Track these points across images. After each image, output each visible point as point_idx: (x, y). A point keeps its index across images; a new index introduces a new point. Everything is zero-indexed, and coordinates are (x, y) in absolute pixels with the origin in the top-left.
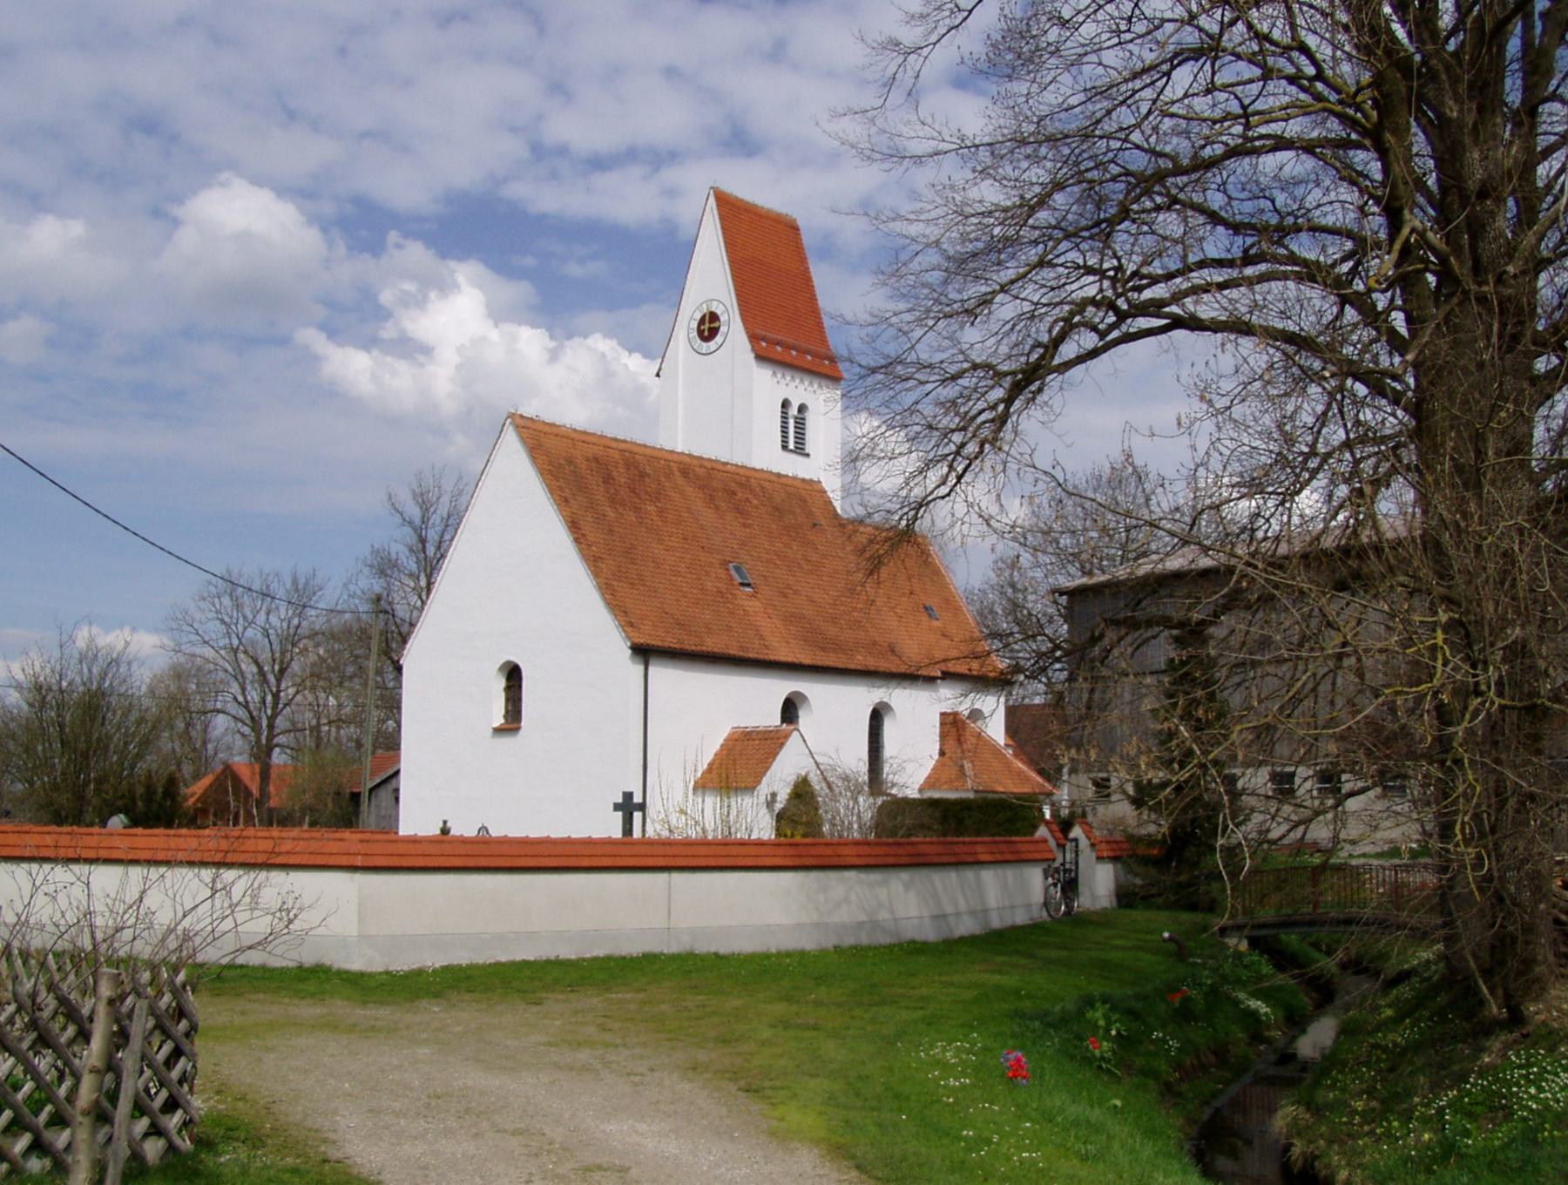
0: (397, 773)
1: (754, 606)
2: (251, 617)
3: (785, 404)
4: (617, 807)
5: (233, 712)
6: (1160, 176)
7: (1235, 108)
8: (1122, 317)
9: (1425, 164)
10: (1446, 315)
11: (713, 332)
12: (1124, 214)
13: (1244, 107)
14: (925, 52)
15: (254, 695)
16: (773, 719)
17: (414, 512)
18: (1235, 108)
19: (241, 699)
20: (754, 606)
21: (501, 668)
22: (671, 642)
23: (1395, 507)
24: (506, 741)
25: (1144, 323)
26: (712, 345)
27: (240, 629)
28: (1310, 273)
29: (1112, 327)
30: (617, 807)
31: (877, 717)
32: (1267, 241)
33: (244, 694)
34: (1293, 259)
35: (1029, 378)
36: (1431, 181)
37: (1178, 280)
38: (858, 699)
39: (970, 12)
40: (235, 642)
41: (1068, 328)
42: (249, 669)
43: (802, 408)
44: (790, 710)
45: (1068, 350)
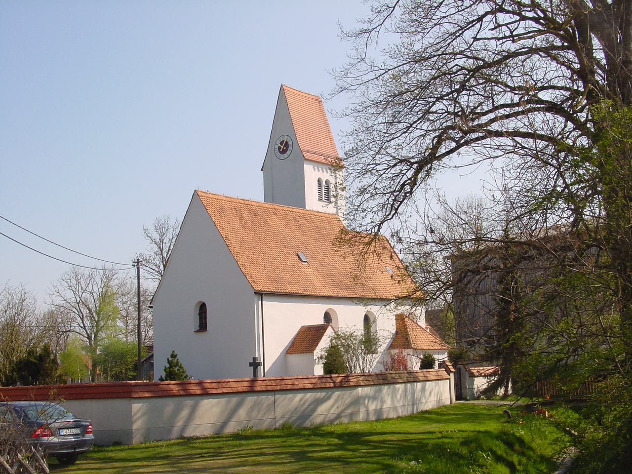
0: (152, 356)
1: (309, 271)
2: (84, 288)
3: (319, 181)
4: (251, 364)
5: (78, 331)
6: (478, 68)
7: (508, 34)
8: (466, 133)
9: (600, 55)
10: (611, 184)
11: (283, 152)
12: (463, 86)
13: (511, 32)
14: (378, 29)
15: (88, 323)
16: (321, 321)
17: (156, 236)
18: (508, 34)
19: (82, 325)
20: (309, 271)
21: (197, 305)
22: (272, 288)
23: (595, 211)
24: (202, 335)
25: (474, 136)
26: (286, 155)
27: (80, 294)
28: (552, 107)
29: (462, 138)
30: (251, 364)
31: (367, 319)
32: (530, 99)
33: (83, 323)
34: (541, 101)
35: (426, 162)
36: (604, 62)
37: (490, 115)
38: (359, 311)
39: (394, 7)
40: (78, 299)
41: (440, 140)
42: (85, 311)
43: (327, 182)
44: (327, 317)
45: (442, 150)
